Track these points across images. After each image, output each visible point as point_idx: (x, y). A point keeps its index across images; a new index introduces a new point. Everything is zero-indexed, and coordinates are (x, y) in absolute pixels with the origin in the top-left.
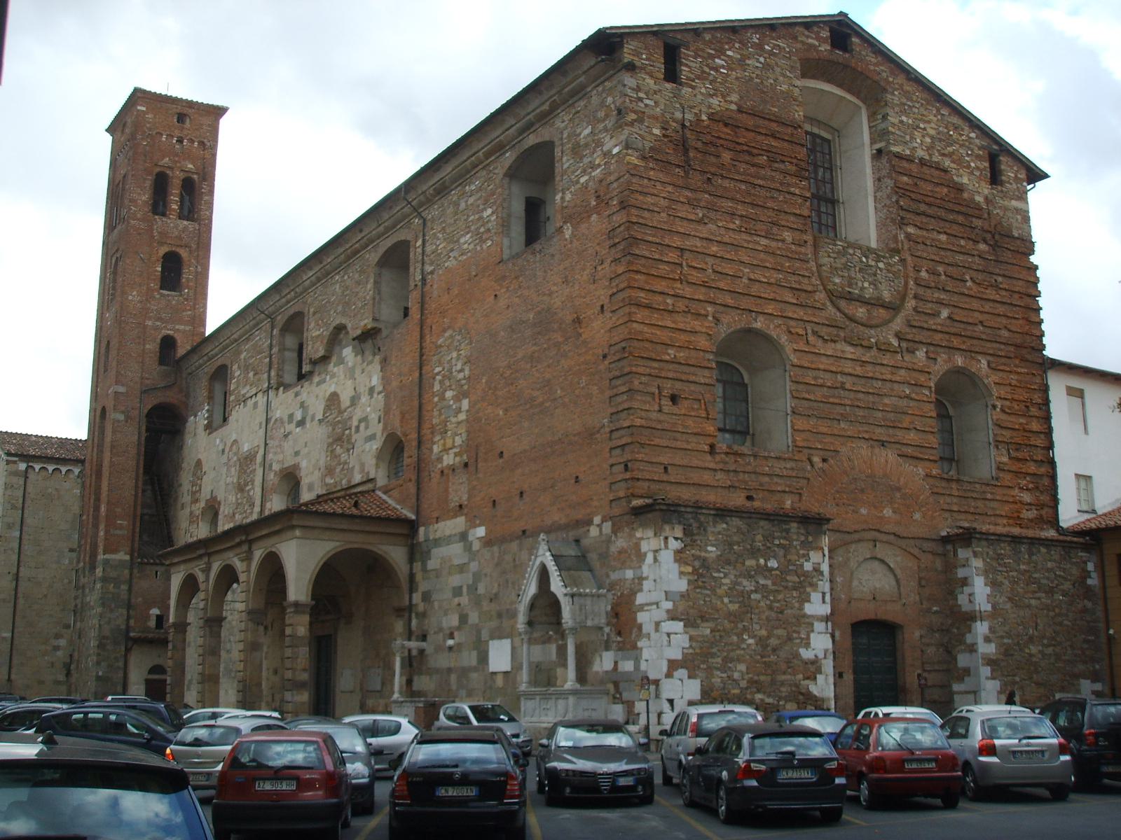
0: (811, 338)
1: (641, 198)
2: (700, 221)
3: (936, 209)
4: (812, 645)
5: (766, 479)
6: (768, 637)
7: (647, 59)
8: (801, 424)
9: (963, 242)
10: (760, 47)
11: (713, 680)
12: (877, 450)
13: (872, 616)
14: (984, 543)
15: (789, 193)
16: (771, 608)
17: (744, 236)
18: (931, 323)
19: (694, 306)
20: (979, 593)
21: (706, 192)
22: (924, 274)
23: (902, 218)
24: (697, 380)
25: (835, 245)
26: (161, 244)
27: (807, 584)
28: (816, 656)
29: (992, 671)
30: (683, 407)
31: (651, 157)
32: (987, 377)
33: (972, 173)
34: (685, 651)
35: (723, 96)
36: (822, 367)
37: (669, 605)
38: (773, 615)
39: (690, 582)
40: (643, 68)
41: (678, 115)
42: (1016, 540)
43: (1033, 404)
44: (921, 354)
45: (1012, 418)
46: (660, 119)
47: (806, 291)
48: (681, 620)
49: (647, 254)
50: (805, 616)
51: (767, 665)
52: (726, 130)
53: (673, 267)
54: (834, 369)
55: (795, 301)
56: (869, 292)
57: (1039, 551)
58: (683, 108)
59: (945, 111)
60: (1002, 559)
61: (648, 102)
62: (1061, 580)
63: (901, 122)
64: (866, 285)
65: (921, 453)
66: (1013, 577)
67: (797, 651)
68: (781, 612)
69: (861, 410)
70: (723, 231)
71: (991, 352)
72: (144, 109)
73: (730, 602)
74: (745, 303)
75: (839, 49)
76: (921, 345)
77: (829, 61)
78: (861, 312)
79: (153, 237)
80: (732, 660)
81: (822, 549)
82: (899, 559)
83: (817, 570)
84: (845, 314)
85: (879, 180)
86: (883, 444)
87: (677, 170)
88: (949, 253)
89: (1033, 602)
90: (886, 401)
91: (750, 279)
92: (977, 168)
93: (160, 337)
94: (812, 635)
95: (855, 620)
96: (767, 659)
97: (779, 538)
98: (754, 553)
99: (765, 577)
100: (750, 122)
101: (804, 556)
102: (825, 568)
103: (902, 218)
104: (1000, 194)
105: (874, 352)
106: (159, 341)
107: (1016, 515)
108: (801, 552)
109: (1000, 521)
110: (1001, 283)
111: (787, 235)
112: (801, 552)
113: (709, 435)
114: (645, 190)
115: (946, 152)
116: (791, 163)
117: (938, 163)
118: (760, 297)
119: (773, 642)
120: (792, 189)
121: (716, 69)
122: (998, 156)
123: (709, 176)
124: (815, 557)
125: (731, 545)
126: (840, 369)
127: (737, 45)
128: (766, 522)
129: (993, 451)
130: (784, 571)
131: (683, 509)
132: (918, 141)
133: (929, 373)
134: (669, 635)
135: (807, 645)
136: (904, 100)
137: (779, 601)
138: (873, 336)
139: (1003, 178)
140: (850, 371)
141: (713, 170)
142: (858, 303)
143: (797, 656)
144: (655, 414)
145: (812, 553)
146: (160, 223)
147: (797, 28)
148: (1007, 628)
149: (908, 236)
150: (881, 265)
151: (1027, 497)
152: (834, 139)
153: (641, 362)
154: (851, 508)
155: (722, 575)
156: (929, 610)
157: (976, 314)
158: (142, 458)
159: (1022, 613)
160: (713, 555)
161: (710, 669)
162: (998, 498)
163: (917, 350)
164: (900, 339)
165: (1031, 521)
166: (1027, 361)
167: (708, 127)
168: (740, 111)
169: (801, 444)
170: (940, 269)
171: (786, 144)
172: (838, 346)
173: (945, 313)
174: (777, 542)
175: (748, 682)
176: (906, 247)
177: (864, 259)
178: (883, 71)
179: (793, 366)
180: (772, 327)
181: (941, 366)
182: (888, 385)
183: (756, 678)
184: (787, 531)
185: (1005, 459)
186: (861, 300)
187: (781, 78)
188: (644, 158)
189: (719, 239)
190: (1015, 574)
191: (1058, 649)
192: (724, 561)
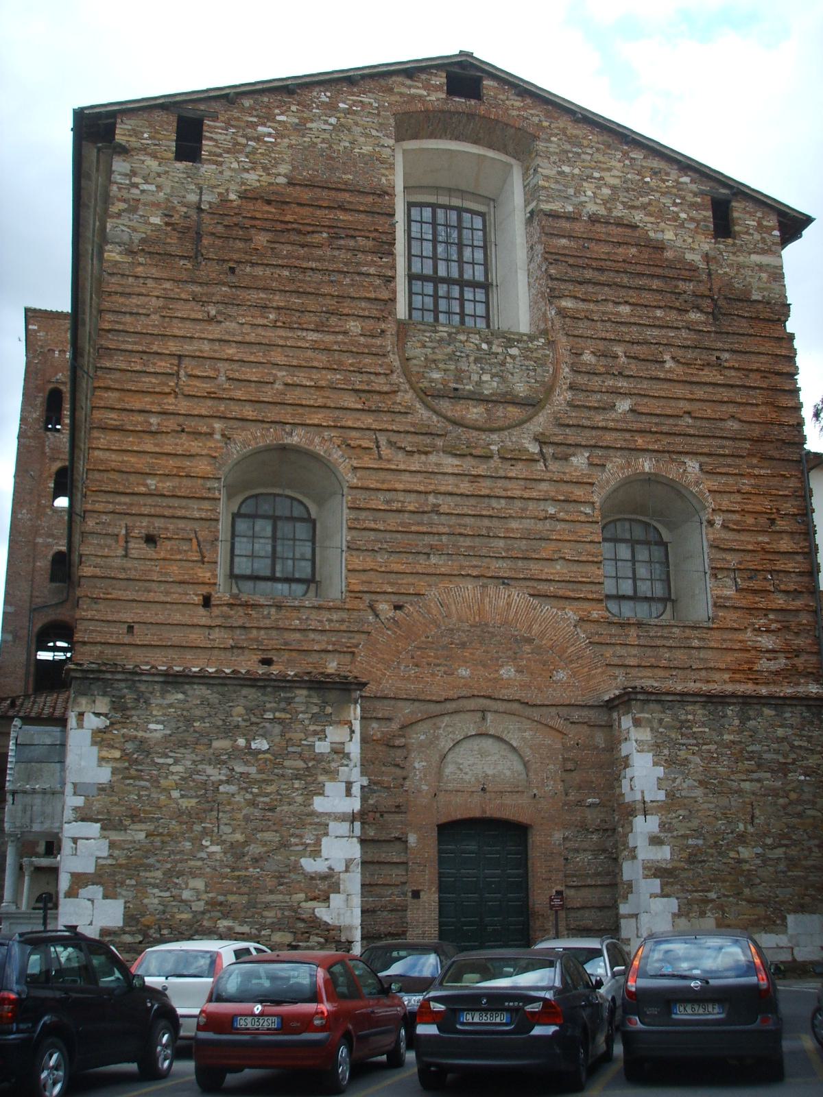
0: (386, 451)
1: (121, 300)
2: (211, 320)
3: (612, 274)
4: (324, 853)
5: (298, 636)
6: (246, 843)
7: (150, 138)
8: (358, 561)
9: (659, 313)
10: (332, 107)
11: (146, 901)
12: (491, 590)
13: (477, 814)
14: (657, 707)
15: (360, 274)
16: (253, 804)
17: (282, 333)
18: (599, 419)
19: (191, 424)
20: (643, 774)
21: (224, 284)
22: (587, 357)
23: (552, 290)
24: (188, 514)
25: (436, 332)
26: (53, 459)
27: (319, 771)
28: (330, 868)
29: (663, 886)
30: (164, 549)
31: (143, 250)
32: (697, 483)
33: (682, 226)
34: (101, 862)
35: (265, 169)
36: (400, 486)
37: (79, 801)
38: (258, 813)
39: (114, 772)
40: (144, 149)
41: (192, 198)
42: (746, 701)
43: (783, 516)
44: (579, 461)
45: (744, 537)
46: (163, 206)
47: (379, 393)
48: (97, 821)
49: (123, 366)
50: (313, 814)
51: (244, 880)
52: (267, 208)
53: (163, 378)
54: (422, 488)
55: (360, 407)
56: (491, 386)
57: (761, 714)
58: (201, 189)
59: (637, 155)
60: (690, 728)
61: (145, 187)
62: (802, 753)
63: (561, 173)
64: (486, 377)
65: (573, 590)
66: (709, 751)
67: (297, 862)
68: (272, 810)
69: (468, 539)
70: (246, 329)
71: (706, 450)
72: (36, 327)
73: (182, 796)
74: (273, 414)
75: (460, 96)
76: (579, 450)
77: (442, 112)
78: (475, 413)
79: (44, 453)
80: (180, 874)
81: (350, 724)
82: (527, 734)
83: (339, 752)
84: (445, 417)
85: (532, 248)
86: (505, 581)
87: (182, 262)
88: (635, 328)
89: (747, 786)
90: (514, 524)
91: (286, 384)
92: (692, 219)
93: (51, 553)
94: (324, 840)
95: (444, 820)
96: (243, 873)
97: (274, 710)
98: (229, 731)
99: (246, 763)
100: (306, 195)
101: (315, 733)
102: (354, 748)
103: (552, 290)
104: (730, 249)
105: (495, 462)
106: (50, 558)
107: (746, 666)
108: (312, 728)
109: (717, 676)
110: (726, 361)
111: (354, 326)
112: (312, 728)
113: (203, 583)
114: (128, 290)
115: (637, 203)
116: (367, 238)
117: (621, 218)
118: (302, 405)
119: (254, 849)
120: (364, 269)
121: (258, 139)
122: (729, 202)
123: (232, 264)
124: (335, 734)
125: (189, 721)
126: (431, 488)
127: (294, 108)
128: (253, 690)
129: (710, 583)
130: (279, 755)
131: (109, 676)
132: (589, 193)
133: (592, 484)
134: (75, 840)
135: (316, 853)
136: (568, 147)
137: (267, 795)
138: (495, 443)
139: (737, 228)
140: (450, 489)
141: (235, 256)
142: (470, 402)
143: (296, 868)
144: (118, 561)
145: (330, 730)
146: (52, 440)
147: (394, 78)
148: (695, 823)
149: (562, 313)
150: (514, 351)
151: (767, 642)
152: (489, 213)
153: (103, 498)
154: (443, 669)
155: (170, 761)
156: (579, 803)
157: (682, 404)
158: (31, 679)
159: (724, 801)
160: (158, 735)
161: (142, 887)
162: (713, 644)
163: (574, 455)
164: (542, 443)
165: (777, 673)
166: (772, 458)
167: (239, 207)
168: (291, 184)
169: (357, 588)
170: (619, 350)
171: (362, 216)
172: (433, 458)
173: (624, 405)
174: (269, 715)
175: (207, 903)
176: (558, 325)
177: (484, 346)
178: (532, 115)
179: (351, 488)
180: (317, 440)
181: (615, 470)
182: (518, 504)
183: (221, 898)
184: (289, 701)
185: (730, 592)
186: (477, 398)
187: (362, 139)
188: (130, 252)
189: (239, 338)
190: (713, 747)
191: (793, 852)
192: (175, 743)
